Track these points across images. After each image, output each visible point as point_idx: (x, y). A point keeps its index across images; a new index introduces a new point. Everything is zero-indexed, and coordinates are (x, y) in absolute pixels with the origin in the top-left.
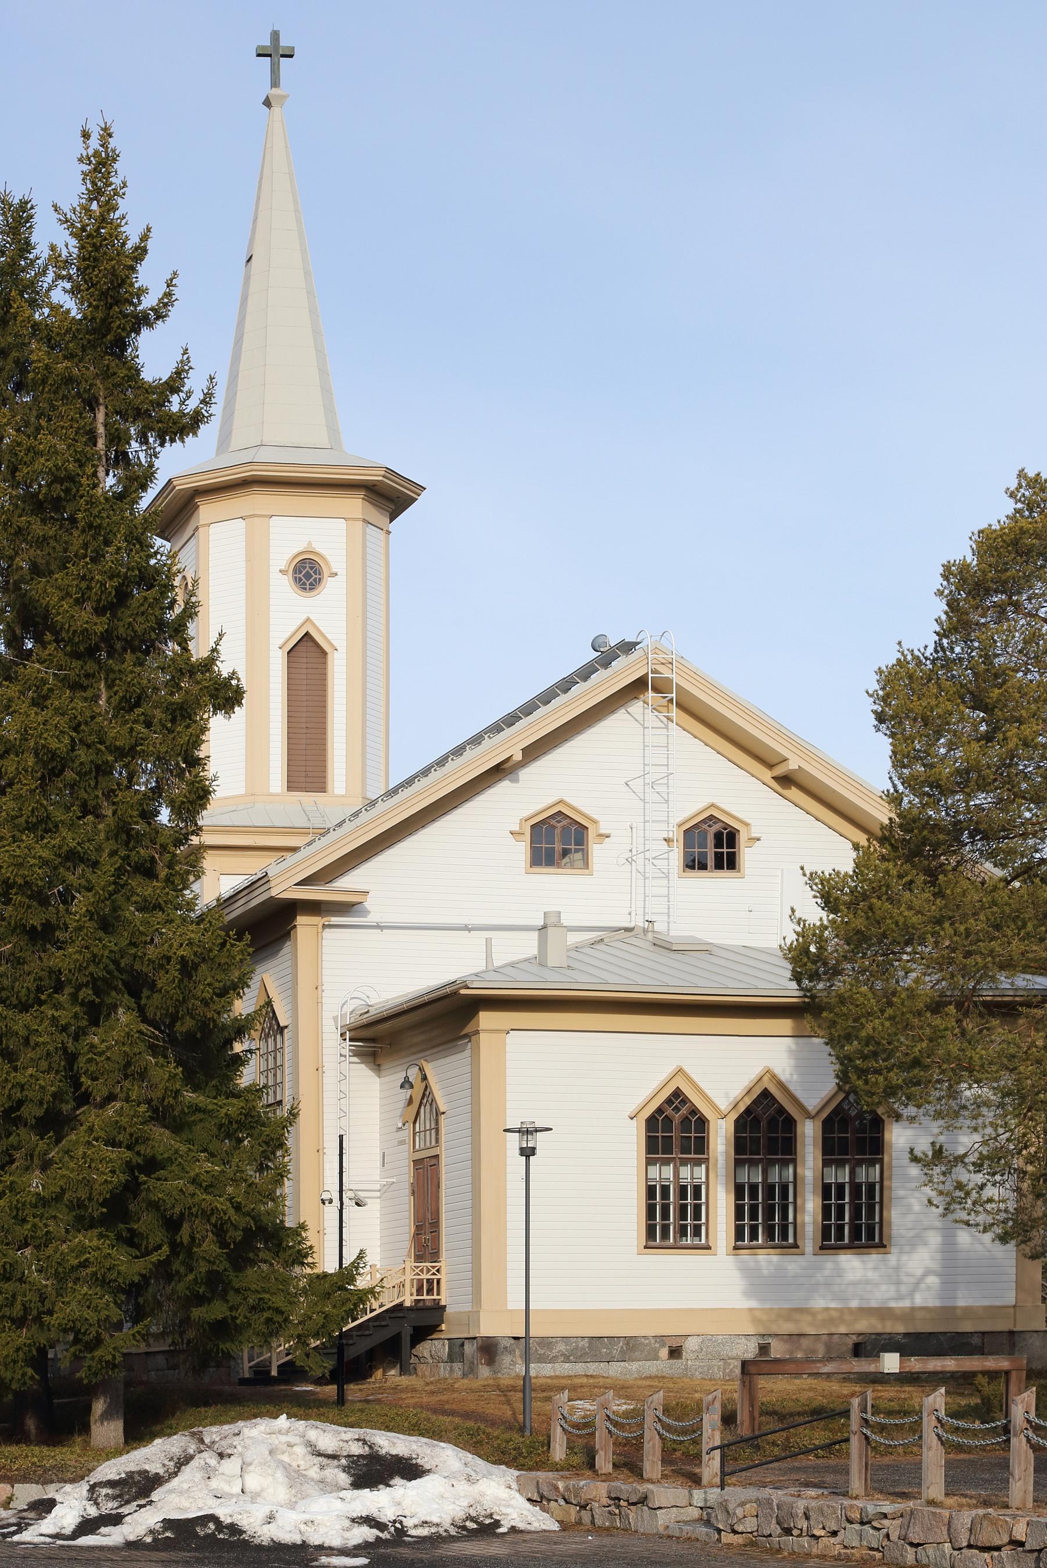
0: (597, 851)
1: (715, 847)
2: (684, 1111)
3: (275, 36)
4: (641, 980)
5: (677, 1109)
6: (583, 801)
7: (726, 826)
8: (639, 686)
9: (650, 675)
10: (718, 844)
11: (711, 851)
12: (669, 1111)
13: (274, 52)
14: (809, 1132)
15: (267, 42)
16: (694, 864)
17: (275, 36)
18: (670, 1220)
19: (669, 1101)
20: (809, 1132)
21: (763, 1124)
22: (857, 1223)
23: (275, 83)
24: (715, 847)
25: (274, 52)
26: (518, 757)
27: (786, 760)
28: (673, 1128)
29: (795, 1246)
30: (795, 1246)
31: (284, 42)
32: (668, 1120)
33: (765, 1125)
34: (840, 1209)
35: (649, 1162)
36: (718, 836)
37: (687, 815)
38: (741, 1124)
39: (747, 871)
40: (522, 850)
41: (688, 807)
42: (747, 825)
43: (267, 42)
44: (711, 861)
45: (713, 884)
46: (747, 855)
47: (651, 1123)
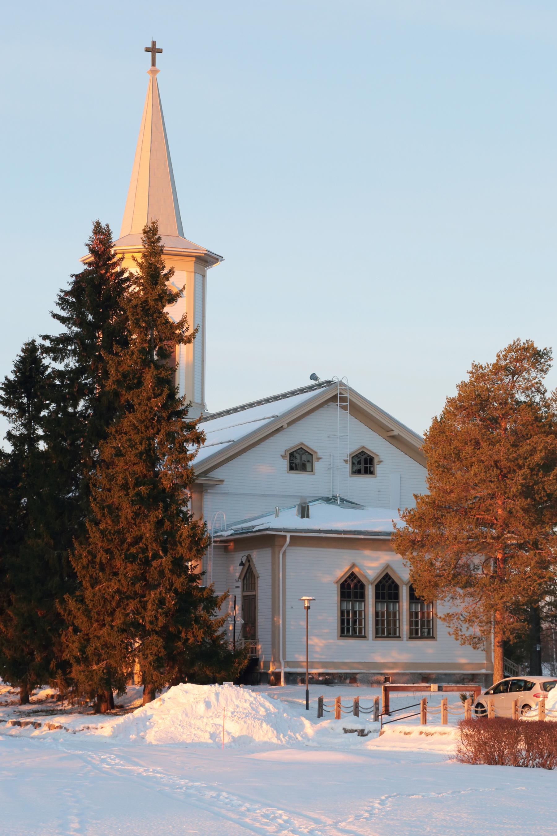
0: (317, 465)
1: (364, 464)
2: (355, 581)
3: (154, 43)
4: (318, 495)
5: (352, 581)
6: (311, 443)
7: (369, 456)
8: (334, 399)
9: (339, 395)
10: (366, 463)
11: (362, 466)
12: (349, 581)
13: (154, 50)
14: (370, 592)
15: (150, 46)
16: (357, 472)
17: (154, 43)
18: (350, 627)
19: (349, 577)
20: (370, 592)
21: (386, 588)
22: (422, 629)
23: (154, 64)
24: (364, 464)
25: (154, 50)
26: (285, 426)
27: (393, 430)
28: (351, 589)
29: (399, 637)
30: (399, 637)
31: (157, 46)
32: (349, 585)
33: (387, 588)
34: (417, 622)
35: (342, 601)
36: (366, 460)
37: (352, 450)
38: (377, 587)
39: (378, 475)
40: (285, 463)
41: (353, 447)
42: (378, 455)
43: (150, 46)
44: (363, 471)
45: (363, 480)
46: (378, 468)
47: (343, 586)
